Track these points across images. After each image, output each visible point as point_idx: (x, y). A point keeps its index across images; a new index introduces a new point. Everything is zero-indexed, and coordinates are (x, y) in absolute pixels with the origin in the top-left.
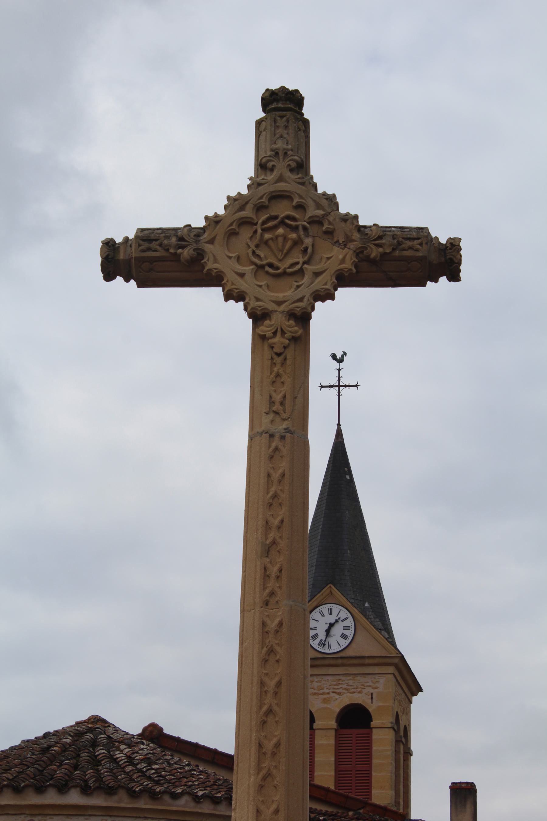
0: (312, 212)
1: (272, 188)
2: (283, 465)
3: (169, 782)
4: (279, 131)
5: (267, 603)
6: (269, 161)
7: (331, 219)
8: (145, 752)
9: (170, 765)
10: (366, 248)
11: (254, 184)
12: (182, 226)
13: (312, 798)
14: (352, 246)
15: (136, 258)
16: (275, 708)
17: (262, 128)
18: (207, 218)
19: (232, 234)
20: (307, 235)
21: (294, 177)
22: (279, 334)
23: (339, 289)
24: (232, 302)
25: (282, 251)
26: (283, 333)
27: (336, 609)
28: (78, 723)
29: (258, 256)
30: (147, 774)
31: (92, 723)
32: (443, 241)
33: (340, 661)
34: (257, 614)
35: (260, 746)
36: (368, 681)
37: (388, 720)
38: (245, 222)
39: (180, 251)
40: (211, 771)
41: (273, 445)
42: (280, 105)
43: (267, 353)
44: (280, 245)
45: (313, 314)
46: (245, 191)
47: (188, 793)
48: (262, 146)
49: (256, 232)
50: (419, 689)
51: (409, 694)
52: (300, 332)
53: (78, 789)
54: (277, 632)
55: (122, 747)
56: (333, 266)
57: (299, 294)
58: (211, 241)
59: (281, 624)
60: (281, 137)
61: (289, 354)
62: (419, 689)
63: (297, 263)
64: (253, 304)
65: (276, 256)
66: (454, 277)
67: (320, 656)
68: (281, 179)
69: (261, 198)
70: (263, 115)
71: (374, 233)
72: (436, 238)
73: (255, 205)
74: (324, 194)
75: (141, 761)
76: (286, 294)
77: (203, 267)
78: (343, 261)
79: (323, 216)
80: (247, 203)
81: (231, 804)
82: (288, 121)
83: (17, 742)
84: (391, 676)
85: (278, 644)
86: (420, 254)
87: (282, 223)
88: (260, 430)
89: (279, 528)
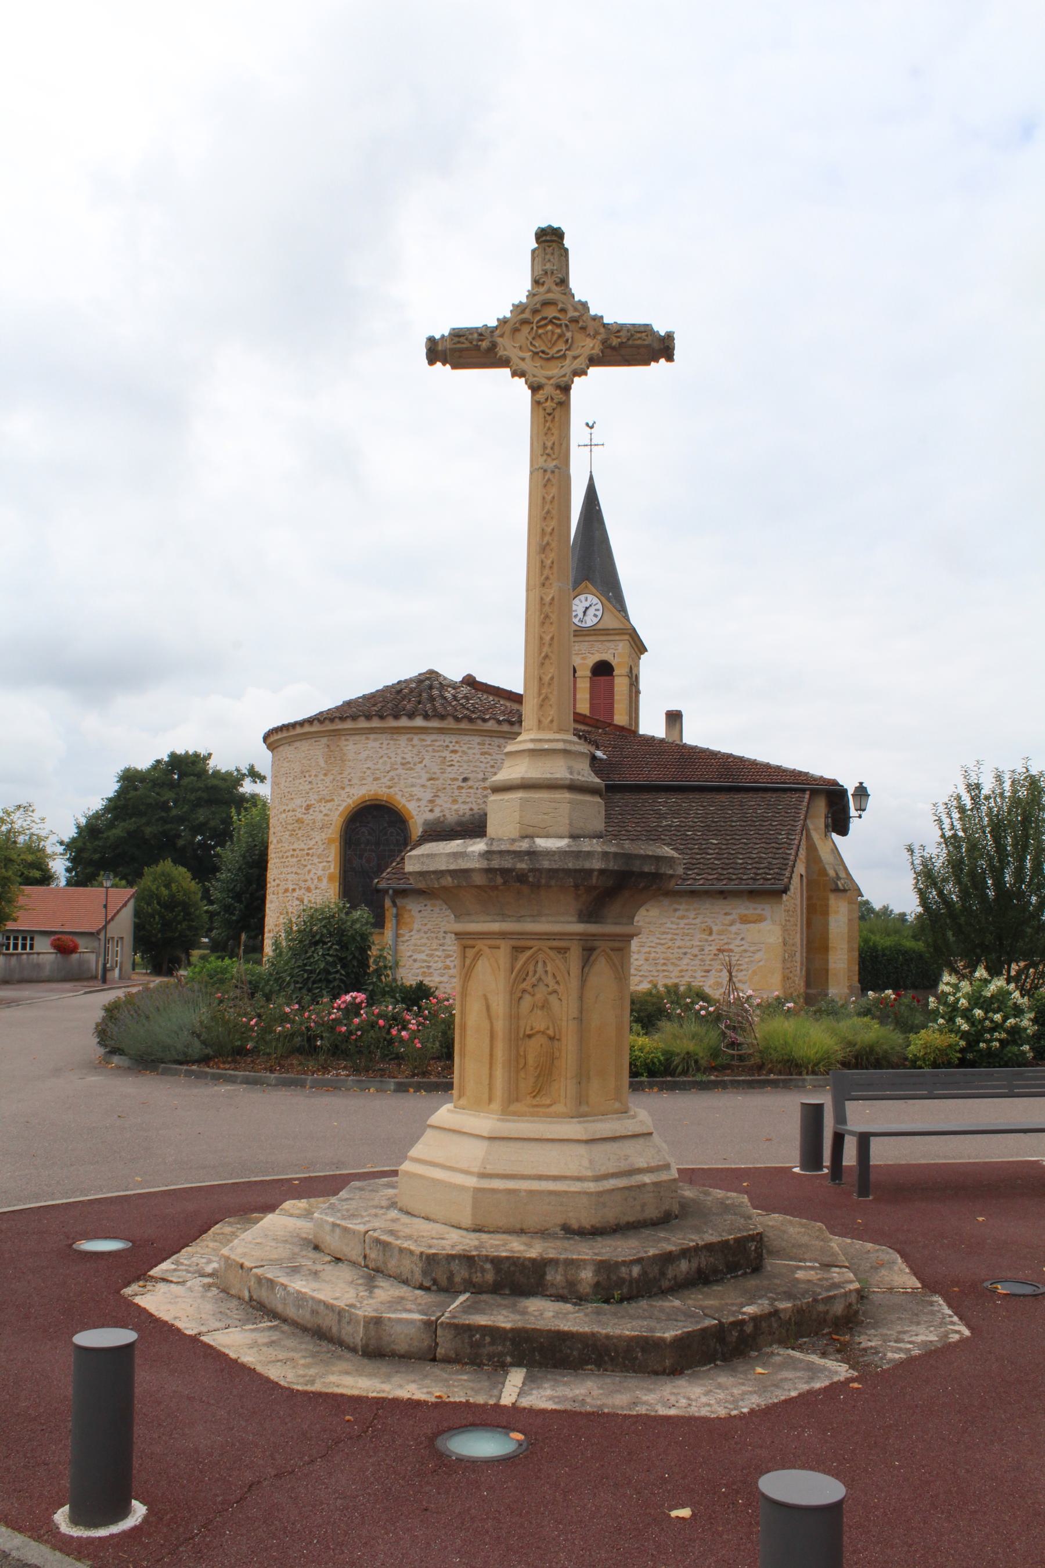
0: (572, 314)
2: (554, 491)
3: (480, 711)
4: (547, 257)
5: (544, 585)
6: (540, 278)
7: (584, 319)
11: (531, 295)
13: (575, 721)
14: (599, 337)
16: (550, 654)
17: (535, 255)
18: (498, 320)
19: (516, 330)
21: (558, 289)
22: (549, 400)
24: (516, 378)
26: (552, 399)
27: (590, 597)
28: (420, 675)
29: (534, 346)
32: (662, 333)
33: (592, 632)
36: (611, 645)
37: (625, 670)
38: (525, 322)
39: (480, 343)
40: (508, 704)
41: (546, 478)
43: (542, 413)
44: (549, 337)
45: (573, 386)
46: (524, 300)
48: (536, 268)
49: (532, 328)
50: (646, 650)
52: (564, 398)
53: (421, 717)
54: (551, 604)
55: (449, 689)
56: (586, 352)
57: (563, 372)
58: (502, 336)
59: (553, 599)
60: (549, 261)
61: (557, 414)
62: (646, 650)
63: (562, 350)
64: (531, 379)
65: (546, 346)
66: (670, 358)
67: (579, 629)
68: (549, 291)
70: (536, 245)
71: (615, 329)
72: (658, 332)
74: (580, 301)
75: (463, 698)
77: (496, 354)
78: (593, 348)
81: (521, 725)
82: (553, 250)
84: (627, 642)
86: (646, 343)
87: (551, 322)
88: (537, 467)
89: (551, 534)
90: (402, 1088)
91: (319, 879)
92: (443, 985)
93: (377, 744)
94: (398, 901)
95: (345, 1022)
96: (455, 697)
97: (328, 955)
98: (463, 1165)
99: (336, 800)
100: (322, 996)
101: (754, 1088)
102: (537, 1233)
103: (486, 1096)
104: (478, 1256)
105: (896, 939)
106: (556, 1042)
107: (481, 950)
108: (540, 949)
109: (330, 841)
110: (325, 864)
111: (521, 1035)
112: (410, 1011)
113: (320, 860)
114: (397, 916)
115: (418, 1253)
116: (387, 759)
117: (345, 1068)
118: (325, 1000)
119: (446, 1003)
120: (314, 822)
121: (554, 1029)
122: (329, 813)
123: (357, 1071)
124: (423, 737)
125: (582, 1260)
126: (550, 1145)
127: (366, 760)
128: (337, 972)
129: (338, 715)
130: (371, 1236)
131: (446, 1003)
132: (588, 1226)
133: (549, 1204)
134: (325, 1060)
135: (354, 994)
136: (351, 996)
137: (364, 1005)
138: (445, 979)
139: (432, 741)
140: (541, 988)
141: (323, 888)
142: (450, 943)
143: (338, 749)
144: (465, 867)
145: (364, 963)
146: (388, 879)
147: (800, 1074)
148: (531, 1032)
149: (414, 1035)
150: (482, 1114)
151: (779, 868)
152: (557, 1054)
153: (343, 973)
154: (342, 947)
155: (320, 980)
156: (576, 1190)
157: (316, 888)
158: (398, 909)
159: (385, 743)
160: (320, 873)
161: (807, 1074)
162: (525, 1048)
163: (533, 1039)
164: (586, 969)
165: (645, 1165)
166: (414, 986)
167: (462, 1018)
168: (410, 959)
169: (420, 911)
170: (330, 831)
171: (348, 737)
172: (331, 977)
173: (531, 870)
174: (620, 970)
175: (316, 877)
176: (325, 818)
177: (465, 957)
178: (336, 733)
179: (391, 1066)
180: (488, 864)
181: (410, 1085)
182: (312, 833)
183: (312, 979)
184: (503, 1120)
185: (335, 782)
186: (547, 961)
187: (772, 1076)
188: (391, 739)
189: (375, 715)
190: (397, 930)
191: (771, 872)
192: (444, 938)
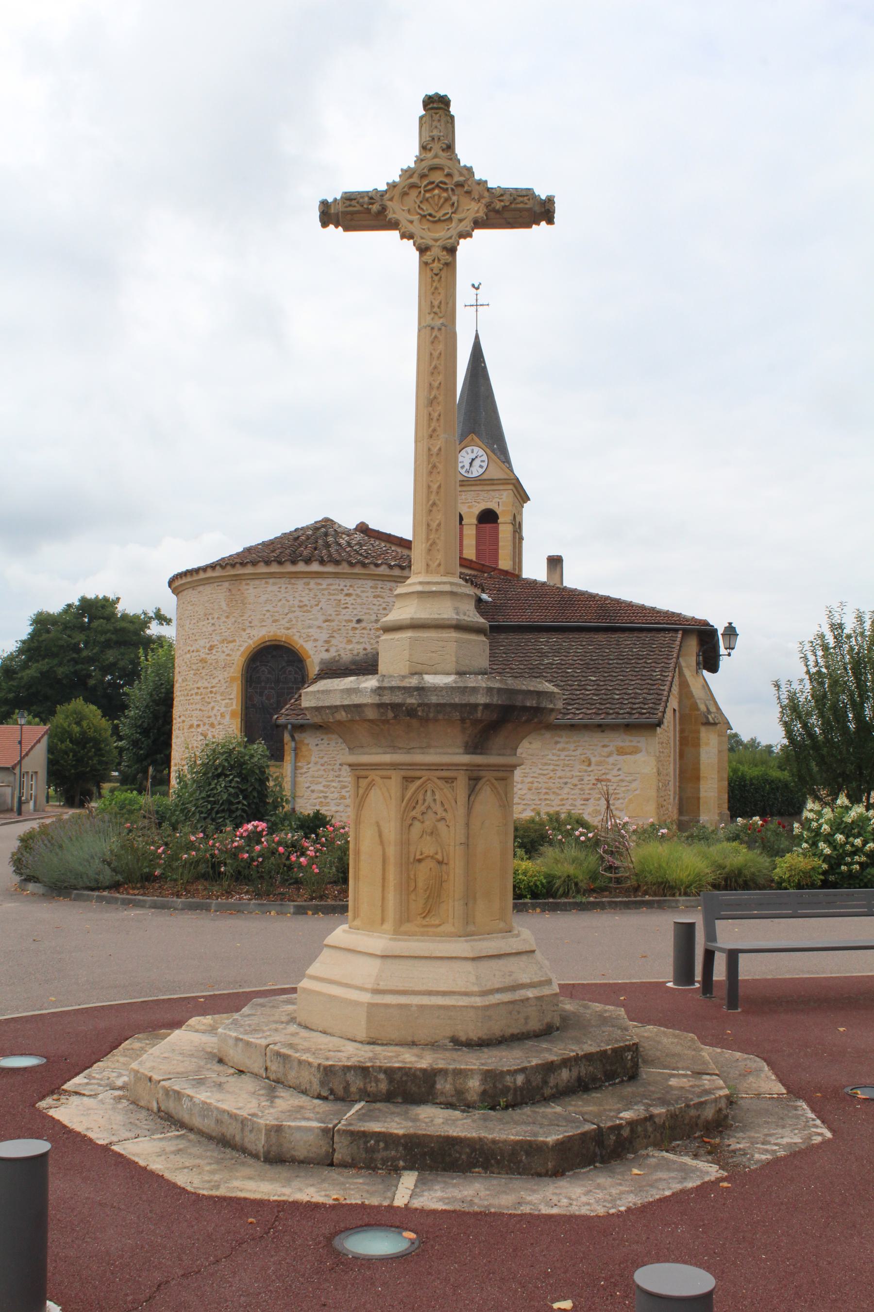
0: (457, 178)
1: (431, 163)
2: (441, 347)
4: (435, 123)
5: (431, 436)
8: (358, 539)
9: (373, 546)
10: (493, 203)
11: (419, 160)
12: (371, 190)
13: (461, 565)
14: (484, 201)
15: (342, 212)
16: (437, 502)
19: (405, 194)
20: (454, 194)
23: (475, 231)
24: (405, 240)
25: (437, 205)
26: (439, 260)
27: (476, 449)
28: (316, 522)
29: (422, 209)
30: (360, 552)
31: (325, 522)
32: (543, 197)
34: (425, 443)
35: (428, 525)
36: (496, 494)
37: (509, 518)
38: (413, 186)
39: (370, 206)
40: (399, 550)
41: (434, 335)
42: (435, 105)
46: (412, 165)
47: (386, 564)
48: (423, 134)
49: (420, 192)
51: (522, 502)
53: (317, 562)
54: (438, 454)
55: (344, 536)
56: (471, 215)
57: (449, 234)
58: (391, 199)
59: (440, 449)
60: (436, 127)
61: (443, 274)
63: (448, 213)
64: (419, 241)
66: (550, 221)
68: (436, 156)
69: (423, 169)
70: (424, 113)
71: (498, 193)
73: (419, 174)
74: (465, 166)
76: (441, 234)
78: (477, 211)
79: (464, 181)
80: (414, 173)
82: (440, 116)
83: (279, 535)
84: (511, 492)
85: (438, 462)
88: (425, 325)
90: (300, 911)
92: (339, 814)
93: (275, 588)
94: (296, 736)
96: (349, 544)
100: (225, 825)
104: (372, 1067)
106: (444, 867)
107: (373, 780)
108: (429, 779)
111: (412, 860)
113: (223, 698)
115: (316, 1064)
116: (285, 602)
117: (247, 893)
119: (342, 831)
122: (231, 653)
123: (258, 895)
124: (319, 581)
126: (439, 963)
127: (265, 603)
128: (239, 803)
129: (239, 561)
130: (272, 1050)
132: (475, 1039)
134: (229, 886)
135: (255, 823)
136: (253, 825)
137: (265, 833)
138: (341, 808)
139: (328, 585)
140: (430, 814)
141: (226, 724)
142: (345, 774)
143: (239, 593)
144: (358, 702)
145: (263, 793)
146: (288, 715)
147: (674, 895)
148: (421, 857)
150: (375, 934)
151: (653, 703)
152: (445, 877)
154: (243, 779)
155: (223, 811)
157: (219, 724)
158: (296, 743)
159: (284, 586)
160: (223, 709)
161: (680, 895)
163: (423, 864)
164: (472, 798)
168: (308, 790)
171: (248, 582)
173: (420, 705)
175: (219, 714)
176: (228, 658)
177: (358, 787)
178: (237, 578)
179: (291, 890)
182: (215, 672)
186: (435, 790)
187: (647, 898)
188: (289, 584)
189: (274, 561)
190: (295, 762)
191: (646, 706)
192: (340, 770)
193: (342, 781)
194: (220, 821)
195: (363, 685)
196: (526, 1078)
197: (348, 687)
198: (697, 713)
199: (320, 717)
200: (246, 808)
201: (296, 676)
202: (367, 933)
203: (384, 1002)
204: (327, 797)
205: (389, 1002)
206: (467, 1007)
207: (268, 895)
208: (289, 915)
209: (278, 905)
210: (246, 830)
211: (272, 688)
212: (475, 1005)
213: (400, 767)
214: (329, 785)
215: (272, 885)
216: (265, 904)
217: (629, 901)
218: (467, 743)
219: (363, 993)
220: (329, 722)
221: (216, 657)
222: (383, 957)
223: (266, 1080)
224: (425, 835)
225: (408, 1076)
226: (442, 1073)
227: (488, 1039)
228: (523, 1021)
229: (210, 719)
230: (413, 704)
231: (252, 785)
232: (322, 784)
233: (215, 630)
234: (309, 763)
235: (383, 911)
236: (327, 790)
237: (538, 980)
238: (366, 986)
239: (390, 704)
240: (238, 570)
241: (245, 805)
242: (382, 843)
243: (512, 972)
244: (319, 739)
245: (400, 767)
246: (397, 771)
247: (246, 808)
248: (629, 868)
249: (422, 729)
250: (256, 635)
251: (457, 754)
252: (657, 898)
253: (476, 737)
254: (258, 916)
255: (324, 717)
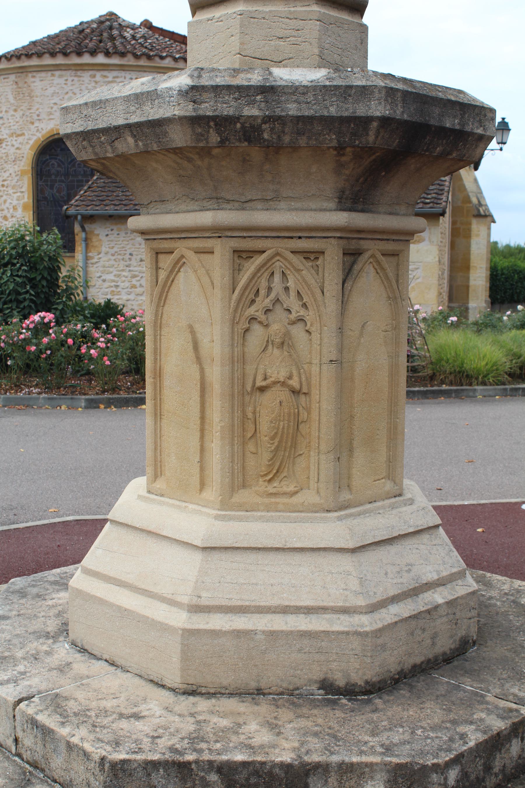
3: (158, 50)
28: (100, 17)
30: (145, 45)
47: (170, 56)
53: (103, 54)
55: (128, 30)
75: (141, 38)
90: (92, 405)
91: (15, 208)
92: (130, 302)
93: (62, 81)
94: (87, 226)
95: (34, 341)
96: (134, 37)
97: (17, 276)
98: (166, 591)
99: (26, 134)
100: (12, 317)
101: (428, 398)
102: (282, 694)
103: (196, 479)
104: (197, 762)
105: (513, 260)
106: (302, 398)
107: (183, 257)
108: (277, 254)
109: (23, 173)
110: (19, 194)
111: (249, 388)
112: (99, 329)
113: (15, 191)
114: (86, 240)
115: (97, 758)
116: (72, 95)
117: (37, 386)
118: (15, 320)
119: (133, 321)
120: (7, 156)
121: (300, 377)
122: (20, 146)
123: (48, 388)
124: (105, 73)
125: (367, 765)
126: (298, 557)
127: (52, 96)
128: (27, 292)
129: (24, 52)
130: (23, 713)
131: (133, 321)
132: (361, 683)
133: (300, 651)
134: (18, 379)
135: (42, 314)
136: (40, 316)
137: (52, 324)
138: (132, 297)
139: (114, 77)
140: (279, 313)
141: (18, 216)
142: (135, 264)
143: (26, 85)
144: (157, 117)
145: (53, 283)
146: (77, 206)
147: (471, 385)
148: (264, 384)
149: (103, 353)
150: (191, 506)
151: (436, 193)
152: (304, 415)
153: (33, 293)
154: (31, 268)
155: (11, 301)
156: (341, 629)
157: (12, 217)
158: (86, 234)
159: (70, 79)
160: (15, 202)
161: (478, 384)
162: (255, 408)
163: (268, 395)
164: (348, 285)
165: (436, 577)
166: (103, 304)
167: (155, 359)
168: (99, 280)
169: (107, 235)
170: (22, 164)
171: (34, 74)
172: (21, 297)
173: (267, 119)
174: (395, 287)
175: (11, 207)
176: (18, 151)
177: (157, 268)
178: (23, 70)
179: (82, 382)
180: (194, 110)
181: (100, 401)
182: (5, 165)
183: (3, 300)
184: (222, 518)
185: (24, 117)
186: (287, 272)
187: (444, 387)
188: (75, 76)
189: (59, 52)
190: (86, 252)
191: (429, 196)
192: (130, 259)
193: (132, 271)
194: (7, 312)
195: (164, 85)
196: (462, 770)
197: (139, 91)
198: (468, 205)
199: (90, 150)
200: (34, 299)
201: (85, 169)
202: (178, 503)
203: (210, 626)
204: (118, 286)
205: (218, 628)
206: (347, 633)
207: (59, 388)
208: (80, 409)
209: (68, 399)
210: (33, 322)
211: (63, 182)
212: (360, 629)
213: (229, 234)
214: (120, 275)
215: (62, 377)
216: (55, 398)
217: (427, 391)
218: (343, 192)
219: (174, 609)
220: (105, 158)
221: (6, 151)
222: (205, 549)
223: (16, 758)
224: (270, 347)
225: (260, 776)
226: (320, 770)
227: (379, 682)
228: (429, 641)
229: (3, 212)
230: (255, 118)
231: (40, 274)
232: (113, 274)
233: (3, 124)
234: (99, 253)
235: (202, 469)
236: (118, 279)
237: (448, 573)
238: (179, 599)
239: (214, 118)
240: (23, 62)
241: (33, 295)
242: (198, 359)
243: (411, 565)
244: (109, 229)
245: (229, 234)
246: (224, 240)
247: (34, 299)
248: (425, 357)
249: (267, 167)
250: (44, 129)
251: (325, 210)
252: (455, 388)
253: (357, 180)
254: (48, 411)
255: (98, 150)
